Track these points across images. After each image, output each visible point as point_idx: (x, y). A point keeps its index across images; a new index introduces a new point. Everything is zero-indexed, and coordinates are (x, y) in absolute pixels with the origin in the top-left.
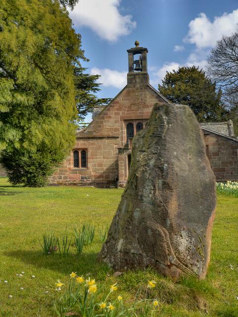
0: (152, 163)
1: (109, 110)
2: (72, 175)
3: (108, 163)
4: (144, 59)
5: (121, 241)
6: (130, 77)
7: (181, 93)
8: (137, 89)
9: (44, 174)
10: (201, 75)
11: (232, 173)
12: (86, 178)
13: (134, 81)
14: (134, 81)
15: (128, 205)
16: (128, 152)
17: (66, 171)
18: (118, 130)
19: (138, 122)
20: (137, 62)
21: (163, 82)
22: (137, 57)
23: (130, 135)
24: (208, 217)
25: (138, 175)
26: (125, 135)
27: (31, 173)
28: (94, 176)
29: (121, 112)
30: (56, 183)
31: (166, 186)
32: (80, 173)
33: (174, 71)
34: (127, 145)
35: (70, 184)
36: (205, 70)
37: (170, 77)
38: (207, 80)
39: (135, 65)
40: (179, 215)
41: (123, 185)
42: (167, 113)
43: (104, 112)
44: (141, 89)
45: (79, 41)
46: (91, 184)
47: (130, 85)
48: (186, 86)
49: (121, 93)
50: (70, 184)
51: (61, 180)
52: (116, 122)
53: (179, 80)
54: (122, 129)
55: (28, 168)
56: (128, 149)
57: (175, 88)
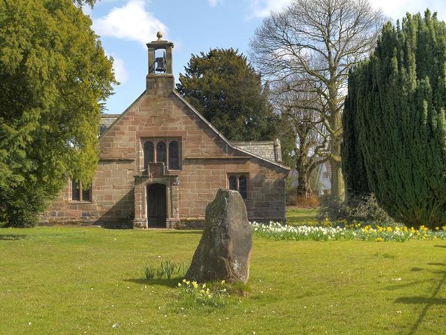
0: (219, 224)
1: (121, 123)
2: (69, 211)
3: (118, 195)
4: (169, 56)
5: (202, 267)
6: (150, 80)
7: (212, 87)
8: (160, 96)
9: (35, 210)
10: (241, 60)
11: (278, 209)
12: (89, 215)
13: (155, 86)
14: (155, 86)
15: (205, 248)
16: (147, 181)
17: (62, 205)
18: (133, 150)
19: (159, 140)
20: (159, 60)
21: (186, 69)
22: (160, 53)
23: (149, 157)
24: (248, 253)
25: (212, 230)
26: (142, 157)
27: (17, 209)
28: (101, 212)
29: (137, 127)
30: (48, 221)
31: (227, 237)
32: (81, 208)
33: (202, 54)
34: (146, 173)
35: (68, 223)
36: (246, 55)
37: (197, 62)
38: (250, 69)
39: (156, 64)
40: (233, 252)
41: (140, 224)
42: (227, 196)
43: (115, 125)
44: (165, 97)
45: (110, 63)
46: (96, 223)
47: (150, 91)
48: (220, 78)
49: (137, 101)
50: (68, 223)
51: (54, 218)
52: (131, 140)
53: (209, 68)
54: (139, 150)
55: (14, 202)
56: (147, 177)
57: (202, 79)
